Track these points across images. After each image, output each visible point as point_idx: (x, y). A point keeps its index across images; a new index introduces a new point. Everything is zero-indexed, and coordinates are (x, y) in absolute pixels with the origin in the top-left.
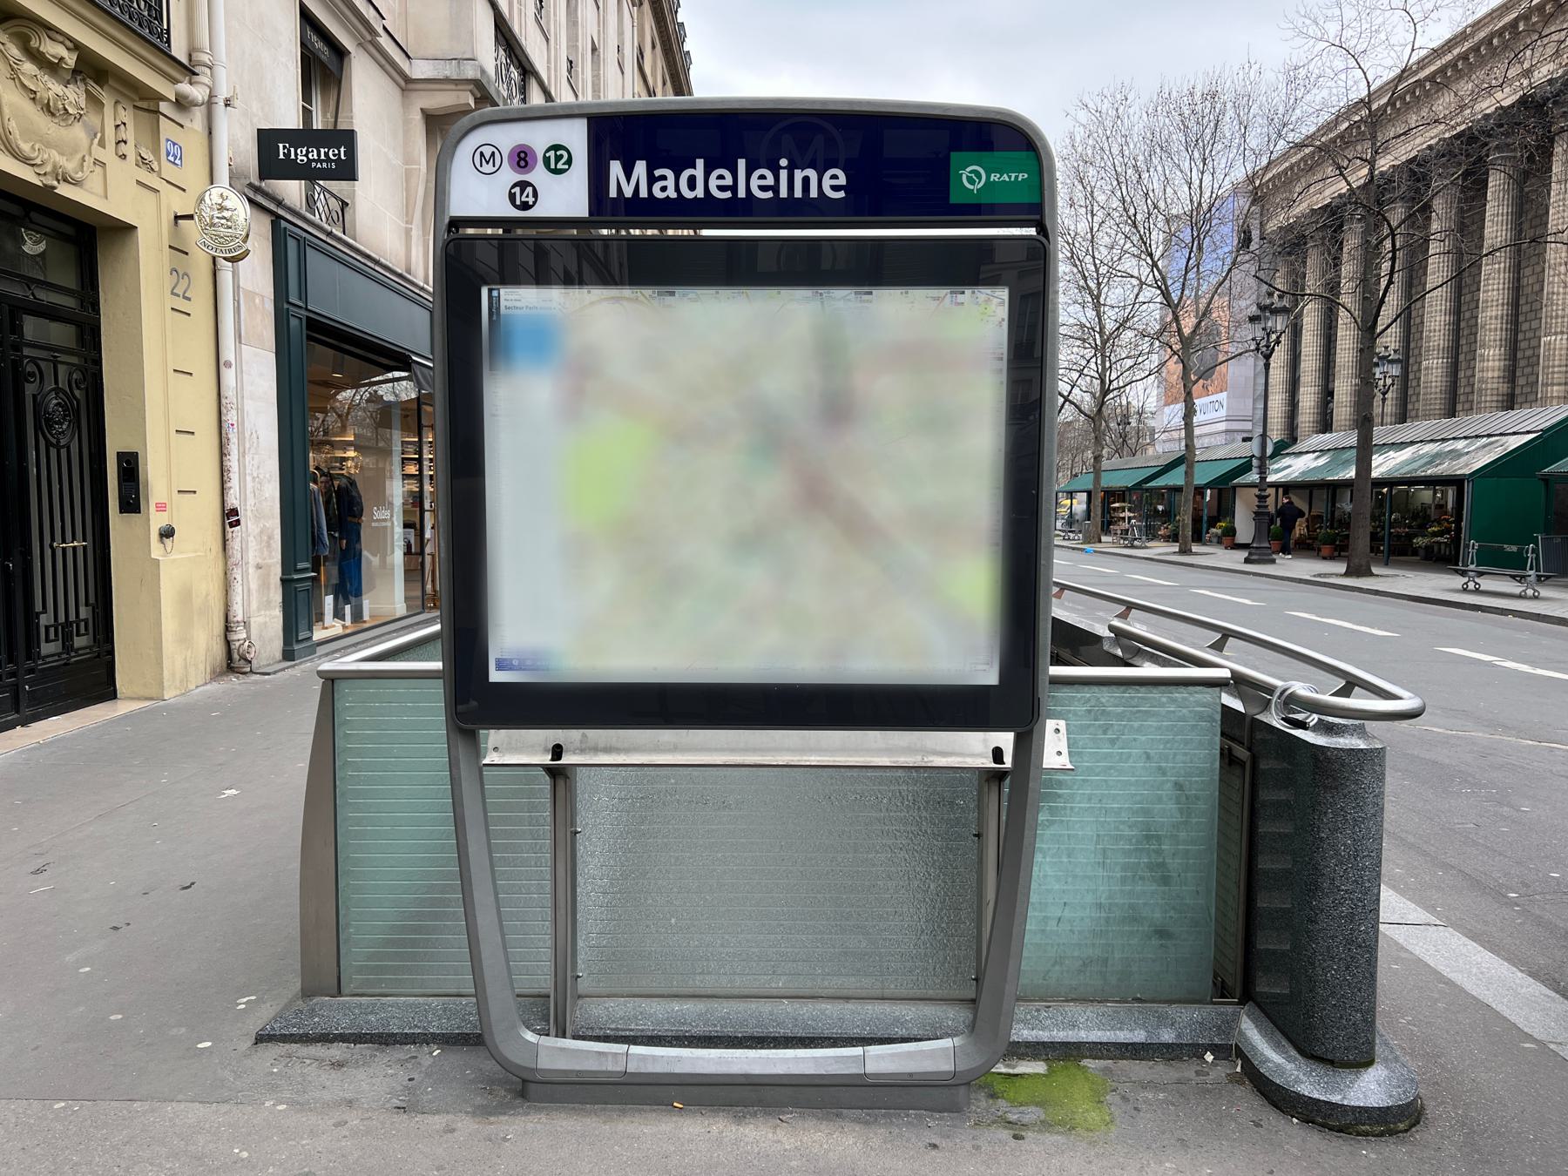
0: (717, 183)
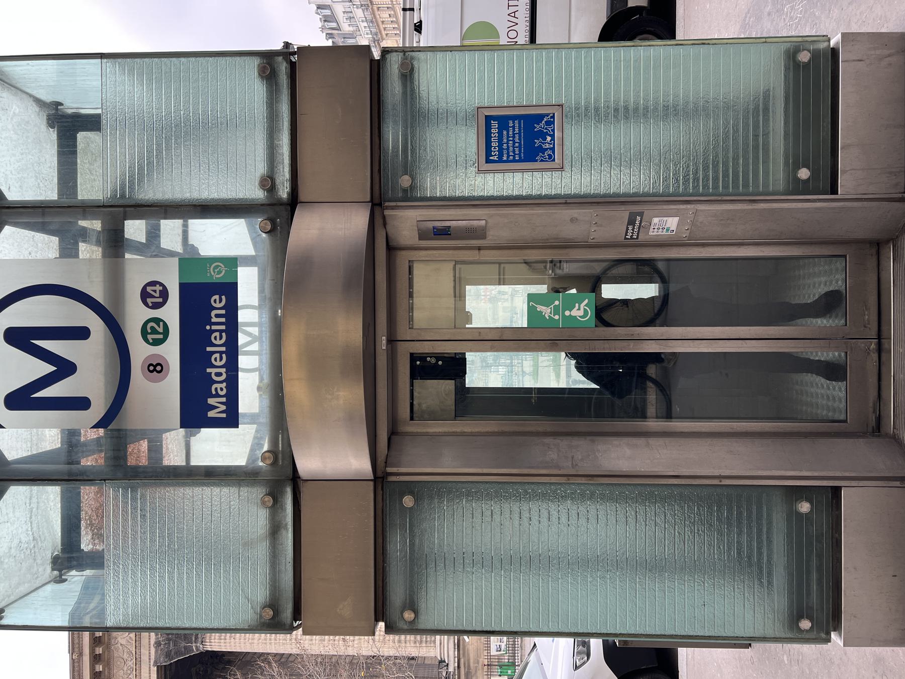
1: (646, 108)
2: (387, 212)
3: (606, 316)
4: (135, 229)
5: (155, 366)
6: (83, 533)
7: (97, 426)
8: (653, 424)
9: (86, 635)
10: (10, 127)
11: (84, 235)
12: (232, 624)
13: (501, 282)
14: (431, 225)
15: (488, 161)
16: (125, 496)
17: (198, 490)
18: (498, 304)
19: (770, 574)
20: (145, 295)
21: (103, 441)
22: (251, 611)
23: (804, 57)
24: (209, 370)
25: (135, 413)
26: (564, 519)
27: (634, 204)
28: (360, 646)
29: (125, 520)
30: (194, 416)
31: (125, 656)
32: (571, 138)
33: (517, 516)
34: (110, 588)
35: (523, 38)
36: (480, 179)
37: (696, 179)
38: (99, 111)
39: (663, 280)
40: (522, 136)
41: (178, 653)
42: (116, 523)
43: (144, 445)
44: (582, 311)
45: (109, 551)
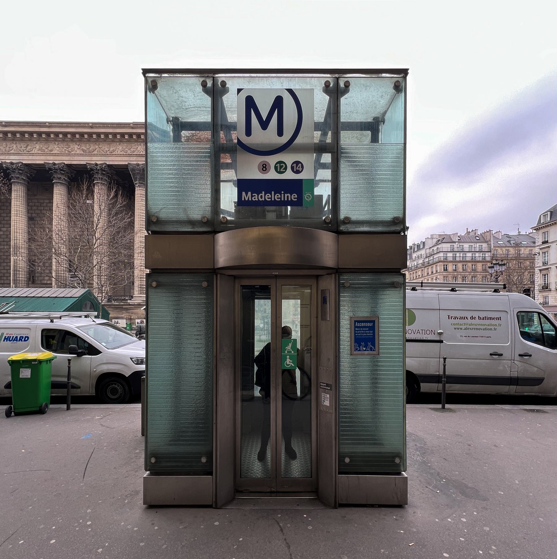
1: (377, 392)
2: (333, 275)
3: (286, 373)
4: (327, 158)
5: (265, 167)
6: (189, 132)
7: (238, 139)
8: (239, 393)
9: (143, 131)
10: (374, 99)
11: (325, 134)
12: (150, 202)
13: (302, 326)
14: (328, 295)
15: (355, 321)
16: (207, 152)
17: (209, 187)
18: (292, 312)
19: (175, 445)
20: (297, 163)
21: (231, 142)
22: (155, 211)
24: (263, 192)
25: (243, 157)
26: (198, 354)
27: (335, 386)
28: (139, 260)
29: (195, 153)
30: (243, 185)
31: (132, 149)
32: (364, 359)
33: (198, 333)
34: (165, 145)
35: (408, 336)
36: (347, 317)
37: (345, 413)
38: (380, 142)
39: (302, 398)
40: (366, 336)
41: (134, 174)
42: (194, 148)
43: (229, 161)
44: (289, 363)
45: (182, 145)
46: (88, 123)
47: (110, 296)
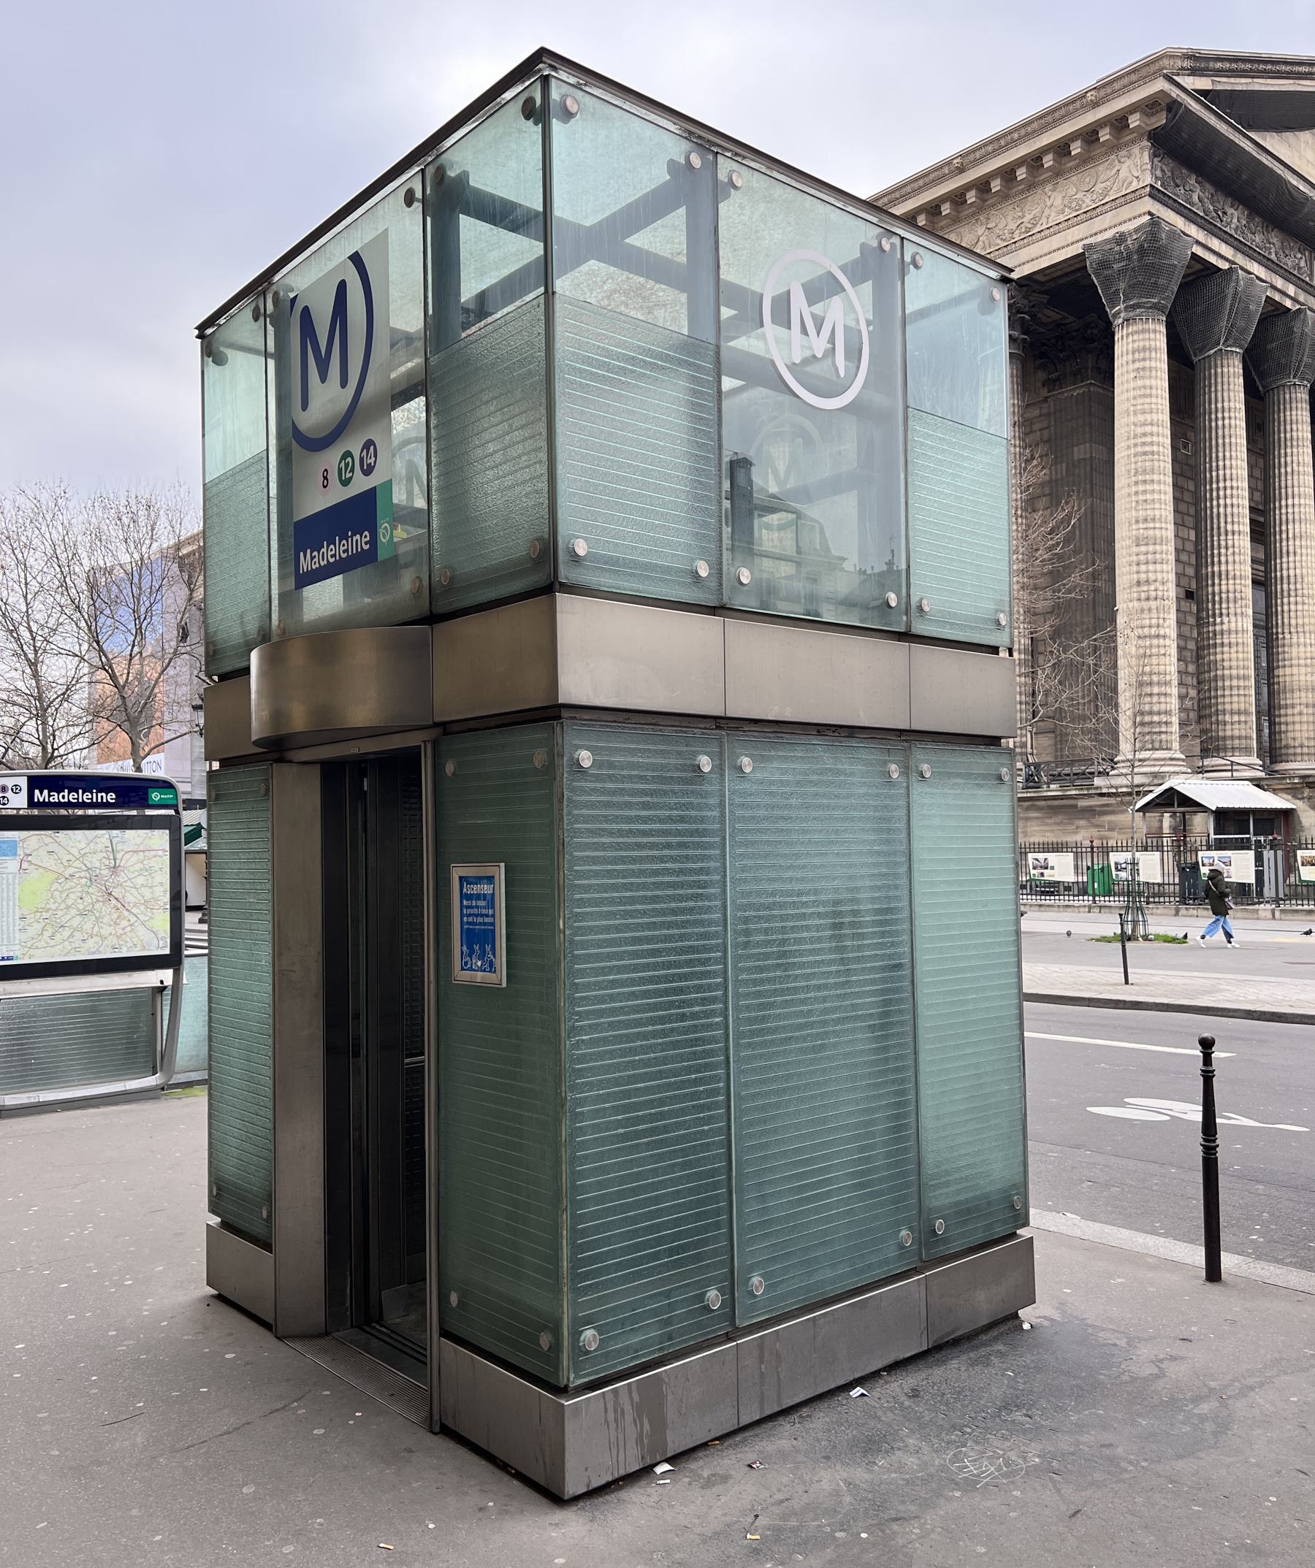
0: (72, 797)
23: (545, 1340)
41: (1107, 282)
46: (948, 163)
47: (1037, 766)
